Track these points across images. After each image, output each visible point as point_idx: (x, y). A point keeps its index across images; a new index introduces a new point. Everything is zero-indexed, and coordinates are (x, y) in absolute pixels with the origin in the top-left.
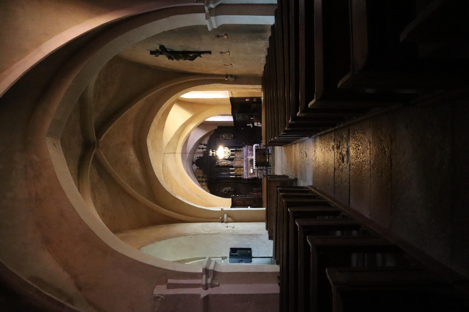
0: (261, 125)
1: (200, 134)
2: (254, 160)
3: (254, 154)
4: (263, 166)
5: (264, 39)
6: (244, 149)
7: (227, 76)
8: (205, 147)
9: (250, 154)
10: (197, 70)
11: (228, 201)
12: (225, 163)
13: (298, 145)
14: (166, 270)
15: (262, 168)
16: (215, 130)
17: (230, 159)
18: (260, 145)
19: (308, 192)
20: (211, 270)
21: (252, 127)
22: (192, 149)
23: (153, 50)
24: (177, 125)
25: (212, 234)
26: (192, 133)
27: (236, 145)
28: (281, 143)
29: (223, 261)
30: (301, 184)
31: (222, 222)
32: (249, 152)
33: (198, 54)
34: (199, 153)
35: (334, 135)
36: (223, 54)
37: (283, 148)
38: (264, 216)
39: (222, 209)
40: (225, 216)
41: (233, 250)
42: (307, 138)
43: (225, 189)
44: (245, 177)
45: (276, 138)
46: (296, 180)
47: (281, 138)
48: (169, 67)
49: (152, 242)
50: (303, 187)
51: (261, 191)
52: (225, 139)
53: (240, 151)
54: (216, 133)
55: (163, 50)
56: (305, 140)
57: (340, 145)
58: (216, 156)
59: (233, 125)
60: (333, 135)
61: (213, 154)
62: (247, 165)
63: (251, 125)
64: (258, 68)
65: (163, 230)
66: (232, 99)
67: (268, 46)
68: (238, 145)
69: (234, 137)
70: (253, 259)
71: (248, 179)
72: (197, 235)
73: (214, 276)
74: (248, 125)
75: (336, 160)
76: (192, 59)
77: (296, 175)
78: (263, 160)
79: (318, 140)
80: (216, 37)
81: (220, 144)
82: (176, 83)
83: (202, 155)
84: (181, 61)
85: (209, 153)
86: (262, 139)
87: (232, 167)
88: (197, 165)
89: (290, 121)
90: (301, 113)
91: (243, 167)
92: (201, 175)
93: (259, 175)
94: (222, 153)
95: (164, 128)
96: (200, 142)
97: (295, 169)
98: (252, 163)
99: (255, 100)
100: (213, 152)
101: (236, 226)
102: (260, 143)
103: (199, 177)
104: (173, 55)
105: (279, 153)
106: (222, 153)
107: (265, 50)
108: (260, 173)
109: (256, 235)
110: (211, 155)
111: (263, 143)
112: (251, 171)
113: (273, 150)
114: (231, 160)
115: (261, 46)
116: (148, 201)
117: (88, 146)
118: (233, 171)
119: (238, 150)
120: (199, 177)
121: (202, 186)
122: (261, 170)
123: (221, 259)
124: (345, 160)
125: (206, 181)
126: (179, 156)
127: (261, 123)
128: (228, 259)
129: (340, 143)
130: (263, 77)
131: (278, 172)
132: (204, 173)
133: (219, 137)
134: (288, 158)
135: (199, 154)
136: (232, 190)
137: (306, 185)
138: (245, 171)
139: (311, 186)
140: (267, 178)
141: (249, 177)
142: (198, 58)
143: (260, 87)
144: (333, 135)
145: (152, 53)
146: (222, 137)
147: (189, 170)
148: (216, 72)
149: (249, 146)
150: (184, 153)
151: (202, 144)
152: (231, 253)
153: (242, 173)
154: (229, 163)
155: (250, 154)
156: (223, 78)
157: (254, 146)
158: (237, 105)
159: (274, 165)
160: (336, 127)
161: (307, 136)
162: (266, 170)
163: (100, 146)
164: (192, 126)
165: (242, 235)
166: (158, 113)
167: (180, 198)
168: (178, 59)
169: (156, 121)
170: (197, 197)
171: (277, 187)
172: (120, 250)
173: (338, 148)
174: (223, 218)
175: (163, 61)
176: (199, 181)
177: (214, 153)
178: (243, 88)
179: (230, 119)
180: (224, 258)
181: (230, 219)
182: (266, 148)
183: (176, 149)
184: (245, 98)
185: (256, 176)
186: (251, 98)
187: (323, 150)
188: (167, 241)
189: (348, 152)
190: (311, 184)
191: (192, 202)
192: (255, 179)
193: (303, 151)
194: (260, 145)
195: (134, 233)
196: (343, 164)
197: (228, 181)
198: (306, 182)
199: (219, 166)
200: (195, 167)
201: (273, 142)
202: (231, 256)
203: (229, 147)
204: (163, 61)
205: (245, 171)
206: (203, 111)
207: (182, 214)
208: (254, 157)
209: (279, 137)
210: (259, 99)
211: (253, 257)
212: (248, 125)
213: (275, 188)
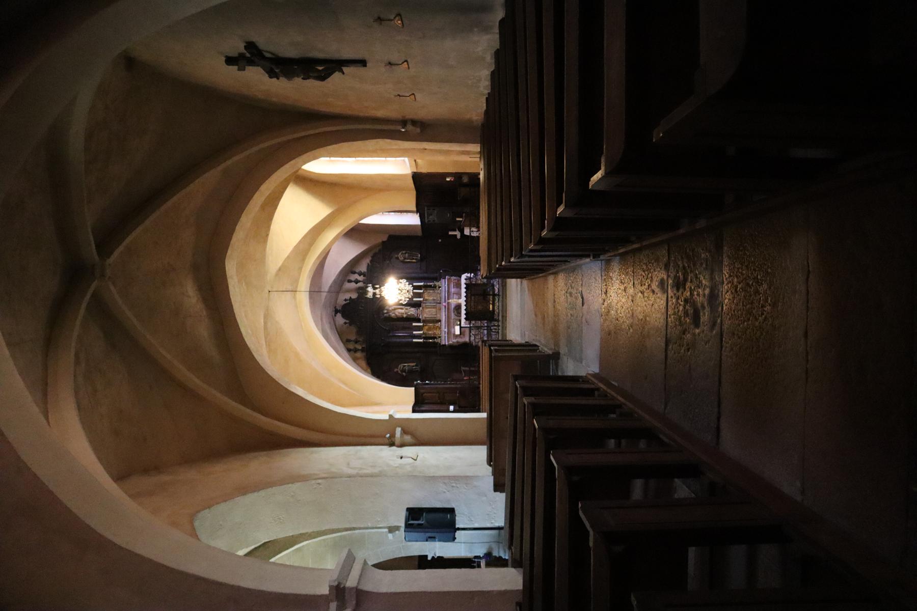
0: (479, 232)
1: (349, 252)
2: (463, 308)
3: (463, 294)
4: (481, 320)
5: (486, 29)
6: (443, 284)
7: (404, 123)
8: (361, 278)
9: (455, 293)
10: (337, 106)
11: (408, 394)
12: (402, 312)
13: (561, 276)
14: (239, 588)
15: (479, 323)
16: (383, 242)
17: (411, 304)
18: (476, 275)
19: (590, 392)
20: (351, 589)
21: (459, 237)
22: (335, 281)
23: (234, 53)
24: (302, 232)
25: (367, 476)
26: (334, 248)
27: (426, 275)
28: (521, 273)
29: (390, 536)
30: (570, 368)
31: (392, 444)
32: (453, 290)
33: (335, 65)
34: (348, 291)
35: (665, 252)
36: (393, 67)
37: (525, 282)
38: (483, 431)
39: (391, 416)
40: (398, 430)
41: (414, 514)
42: (588, 260)
43: (401, 366)
44: (445, 341)
45: (512, 260)
46: (556, 356)
47: (527, 259)
48: (274, 99)
49: (227, 497)
50: (575, 379)
51: (477, 373)
52: (403, 262)
53: (435, 287)
54: (386, 250)
55: (252, 55)
56: (580, 266)
57: (685, 280)
58: (382, 298)
59: (420, 233)
60: (663, 252)
61: (374, 294)
62: (448, 317)
63: (458, 233)
64: (473, 104)
65: (257, 465)
66: (417, 177)
67: (497, 45)
68: (432, 275)
69: (422, 260)
70: (458, 534)
71: (451, 347)
72: (332, 477)
73: (358, 604)
74: (450, 233)
75: (671, 319)
76: (322, 77)
77: (557, 344)
78: (484, 307)
79: (616, 265)
80: (375, 21)
81: (389, 274)
82: (290, 137)
83: (354, 296)
84: (298, 81)
85: (366, 292)
86: (478, 262)
87: (418, 320)
88: (344, 316)
89: (560, 209)
90: (607, 174)
91: (440, 321)
92: (353, 337)
93: (472, 338)
94: (394, 291)
95: (267, 235)
96: (351, 268)
97: (555, 332)
98: (459, 314)
99: (465, 180)
100: (375, 288)
101: (421, 456)
102: (475, 270)
103: (348, 341)
104: (280, 66)
105: (517, 296)
106: (394, 291)
107: (489, 58)
108: (475, 335)
109: (467, 477)
110: (370, 295)
111: (483, 270)
112: (457, 330)
113: (504, 286)
114: (417, 305)
115: (480, 49)
116: (226, 399)
117: (76, 274)
118: (419, 328)
119: (430, 286)
120: (348, 341)
121: (355, 360)
122: (478, 328)
123: (386, 530)
124: (705, 317)
125: (363, 350)
126: (304, 298)
127: (478, 227)
128: (403, 529)
129: (685, 275)
130: (483, 125)
131: (515, 334)
132: (359, 333)
133: (390, 259)
134: (536, 305)
135: (349, 294)
136: (418, 368)
137: (582, 373)
138: (444, 329)
139: (595, 375)
140: (491, 351)
141: (453, 341)
142: (337, 76)
143: (476, 148)
144: (663, 252)
145: (230, 61)
146: (397, 258)
147: (327, 327)
148: (381, 113)
149: (453, 278)
150: (314, 291)
151: (354, 273)
152: (407, 520)
153: (437, 332)
154: (412, 311)
155: (455, 293)
156: (392, 127)
157: (464, 276)
158: (429, 190)
159: (504, 317)
160: (681, 231)
161: (588, 256)
162: (489, 329)
163: (108, 272)
164: (331, 235)
165: (433, 479)
166: (252, 202)
167: (300, 392)
168: (289, 75)
169: (246, 220)
170: (343, 386)
171: (516, 378)
172: (122, 538)
173: (679, 285)
174: (393, 435)
175: (256, 81)
176: (349, 350)
177: (377, 291)
178: (440, 152)
179: (413, 220)
180: (392, 529)
181: (408, 438)
182: (489, 282)
183: (296, 281)
184: (444, 175)
185: (467, 339)
186: (458, 176)
187: (631, 291)
188: (262, 493)
189: (713, 297)
190: (595, 368)
191: (329, 401)
192: (465, 345)
193: (574, 291)
194: (476, 275)
195: (190, 474)
196: (697, 331)
197: (409, 350)
198: (583, 363)
199: (390, 319)
200: (340, 320)
201: (505, 269)
202: (408, 526)
203: (410, 280)
204: (256, 81)
205: (444, 329)
206: (355, 202)
207: (304, 428)
208: (462, 301)
209: (522, 256)
210: (474, 177)
211: (459, 529)
212: (450, 233)
213: (511, 380)
